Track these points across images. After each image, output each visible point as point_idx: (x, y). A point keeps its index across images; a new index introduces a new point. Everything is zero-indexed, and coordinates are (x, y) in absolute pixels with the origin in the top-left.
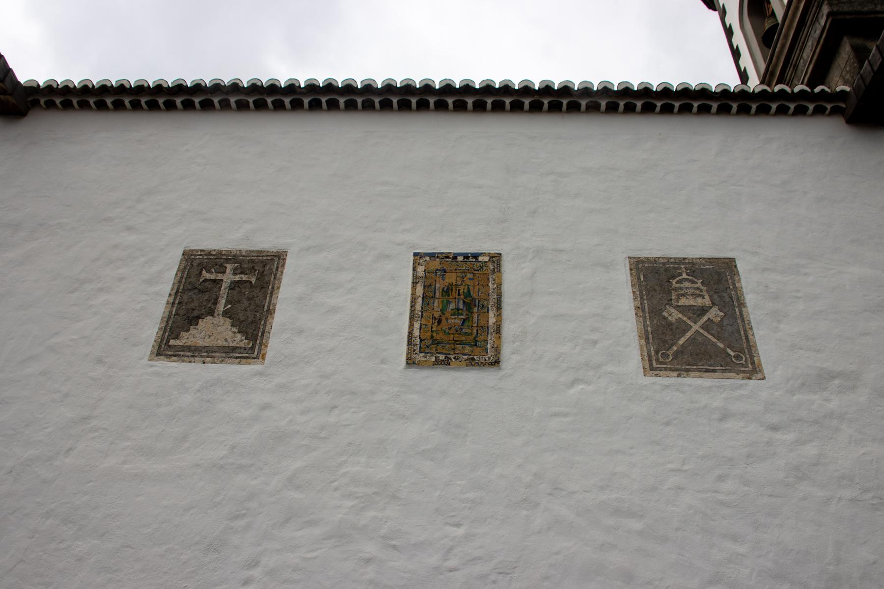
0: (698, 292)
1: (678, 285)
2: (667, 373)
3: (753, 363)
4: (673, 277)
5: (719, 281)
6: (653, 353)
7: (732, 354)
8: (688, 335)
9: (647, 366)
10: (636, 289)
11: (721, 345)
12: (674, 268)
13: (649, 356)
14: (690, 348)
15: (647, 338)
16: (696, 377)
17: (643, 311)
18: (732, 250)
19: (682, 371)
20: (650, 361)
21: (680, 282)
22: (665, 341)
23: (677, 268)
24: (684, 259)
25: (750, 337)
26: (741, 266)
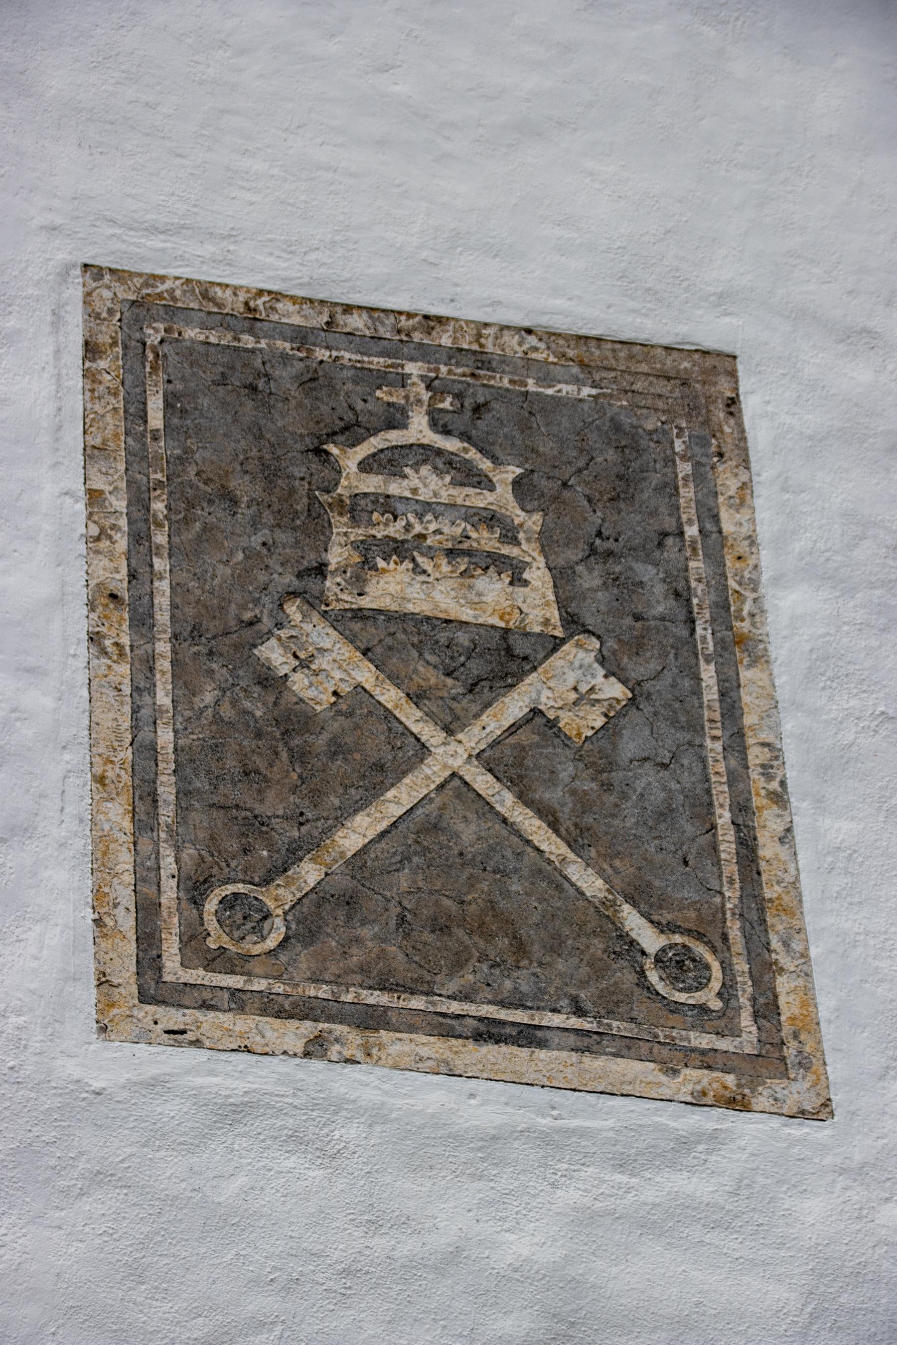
0: (486, 540)
1: (372, 484)
2: (244, 1024)
3: (767, 1010)
4: (351, 431)
5: (622, 489)
6: (170, 892)
7: (651, 940)
8: (400, 798)
9: (125, 973)
10: (112, 479)
11: (592, 885)
12: (362, 373)
13: (147, 910)
14: (403, 880)
15: (145, 795)
16: (418, 1065)
17: (142, 621)
18: (723, 300)
19: (340, 1022)
20: (148, 940)
21: (387, 463)
22: (256, 826)
23: (381, 379)
24: (432, 322)
25: (768, 849)
26: (766, 410)
